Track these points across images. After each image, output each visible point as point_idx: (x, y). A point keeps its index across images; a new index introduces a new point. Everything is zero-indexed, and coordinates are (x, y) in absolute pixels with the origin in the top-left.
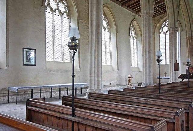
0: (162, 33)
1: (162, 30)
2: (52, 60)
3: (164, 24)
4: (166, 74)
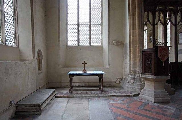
2: (88, 44)
4: (85, 64)
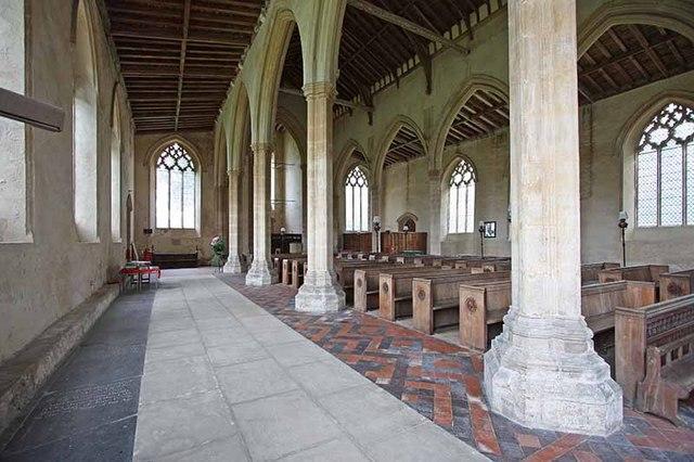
0: (648, 148)
1: (163, 162)
2: (167, 227)
3: (655, 119)
